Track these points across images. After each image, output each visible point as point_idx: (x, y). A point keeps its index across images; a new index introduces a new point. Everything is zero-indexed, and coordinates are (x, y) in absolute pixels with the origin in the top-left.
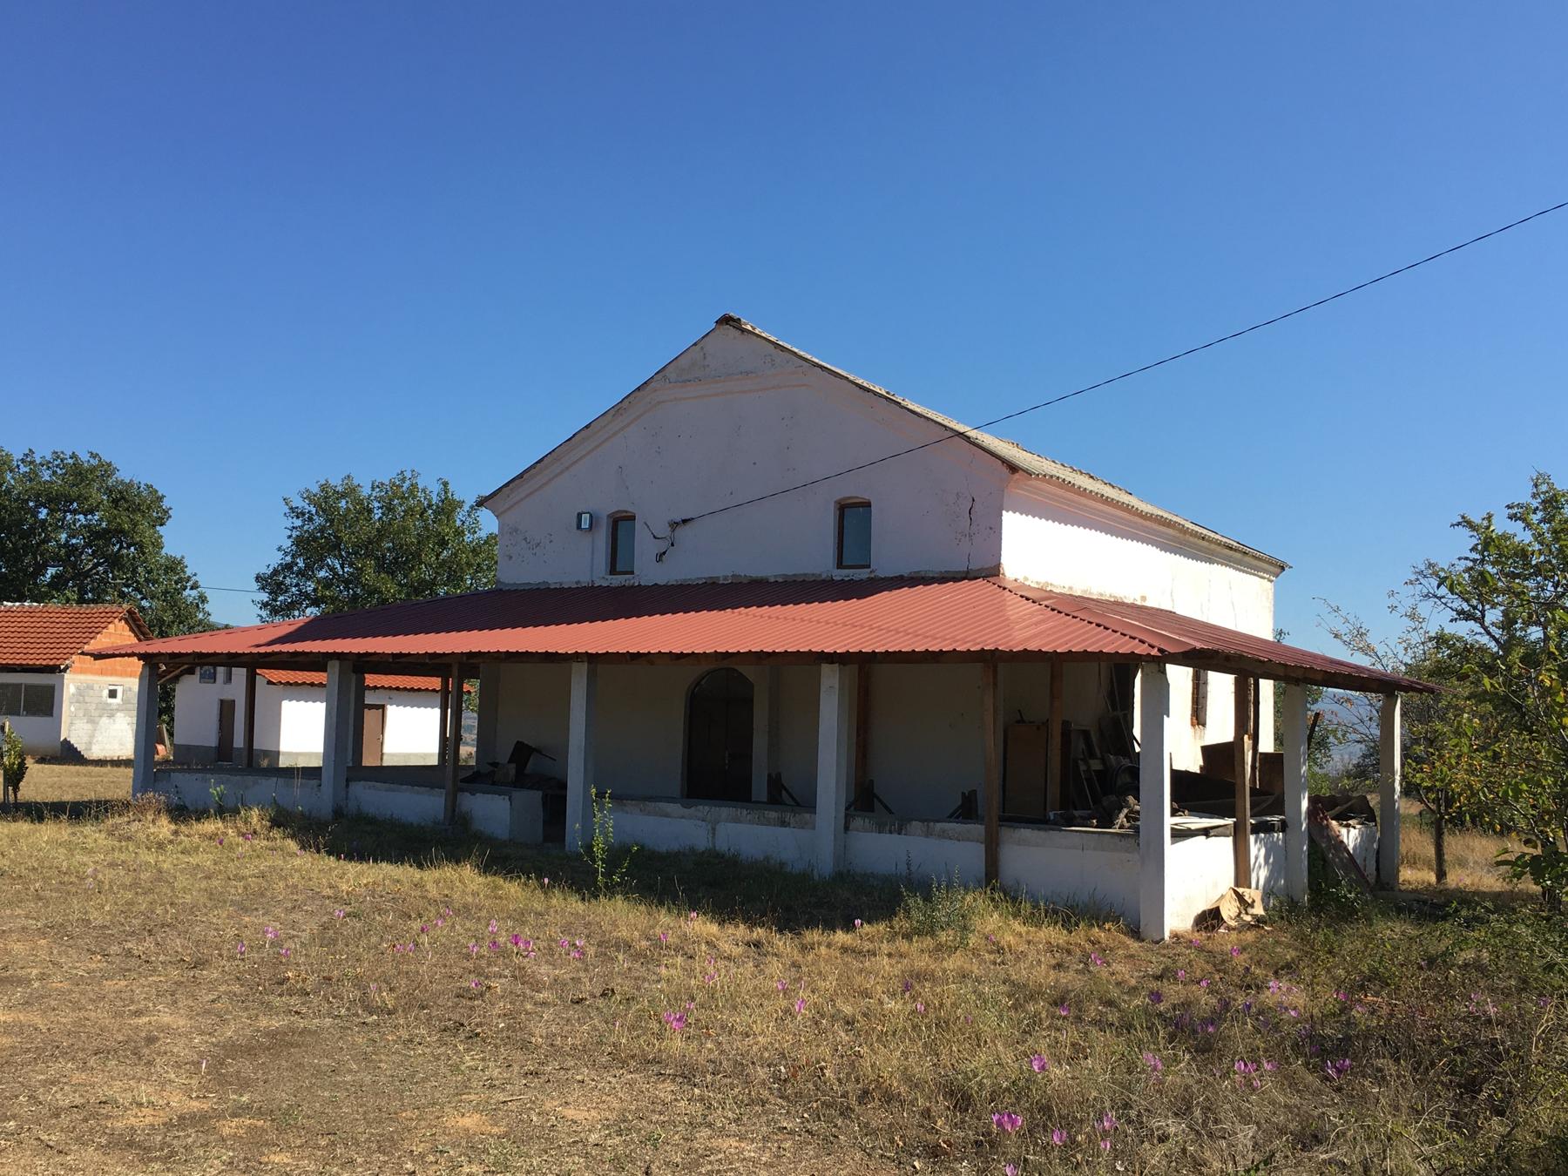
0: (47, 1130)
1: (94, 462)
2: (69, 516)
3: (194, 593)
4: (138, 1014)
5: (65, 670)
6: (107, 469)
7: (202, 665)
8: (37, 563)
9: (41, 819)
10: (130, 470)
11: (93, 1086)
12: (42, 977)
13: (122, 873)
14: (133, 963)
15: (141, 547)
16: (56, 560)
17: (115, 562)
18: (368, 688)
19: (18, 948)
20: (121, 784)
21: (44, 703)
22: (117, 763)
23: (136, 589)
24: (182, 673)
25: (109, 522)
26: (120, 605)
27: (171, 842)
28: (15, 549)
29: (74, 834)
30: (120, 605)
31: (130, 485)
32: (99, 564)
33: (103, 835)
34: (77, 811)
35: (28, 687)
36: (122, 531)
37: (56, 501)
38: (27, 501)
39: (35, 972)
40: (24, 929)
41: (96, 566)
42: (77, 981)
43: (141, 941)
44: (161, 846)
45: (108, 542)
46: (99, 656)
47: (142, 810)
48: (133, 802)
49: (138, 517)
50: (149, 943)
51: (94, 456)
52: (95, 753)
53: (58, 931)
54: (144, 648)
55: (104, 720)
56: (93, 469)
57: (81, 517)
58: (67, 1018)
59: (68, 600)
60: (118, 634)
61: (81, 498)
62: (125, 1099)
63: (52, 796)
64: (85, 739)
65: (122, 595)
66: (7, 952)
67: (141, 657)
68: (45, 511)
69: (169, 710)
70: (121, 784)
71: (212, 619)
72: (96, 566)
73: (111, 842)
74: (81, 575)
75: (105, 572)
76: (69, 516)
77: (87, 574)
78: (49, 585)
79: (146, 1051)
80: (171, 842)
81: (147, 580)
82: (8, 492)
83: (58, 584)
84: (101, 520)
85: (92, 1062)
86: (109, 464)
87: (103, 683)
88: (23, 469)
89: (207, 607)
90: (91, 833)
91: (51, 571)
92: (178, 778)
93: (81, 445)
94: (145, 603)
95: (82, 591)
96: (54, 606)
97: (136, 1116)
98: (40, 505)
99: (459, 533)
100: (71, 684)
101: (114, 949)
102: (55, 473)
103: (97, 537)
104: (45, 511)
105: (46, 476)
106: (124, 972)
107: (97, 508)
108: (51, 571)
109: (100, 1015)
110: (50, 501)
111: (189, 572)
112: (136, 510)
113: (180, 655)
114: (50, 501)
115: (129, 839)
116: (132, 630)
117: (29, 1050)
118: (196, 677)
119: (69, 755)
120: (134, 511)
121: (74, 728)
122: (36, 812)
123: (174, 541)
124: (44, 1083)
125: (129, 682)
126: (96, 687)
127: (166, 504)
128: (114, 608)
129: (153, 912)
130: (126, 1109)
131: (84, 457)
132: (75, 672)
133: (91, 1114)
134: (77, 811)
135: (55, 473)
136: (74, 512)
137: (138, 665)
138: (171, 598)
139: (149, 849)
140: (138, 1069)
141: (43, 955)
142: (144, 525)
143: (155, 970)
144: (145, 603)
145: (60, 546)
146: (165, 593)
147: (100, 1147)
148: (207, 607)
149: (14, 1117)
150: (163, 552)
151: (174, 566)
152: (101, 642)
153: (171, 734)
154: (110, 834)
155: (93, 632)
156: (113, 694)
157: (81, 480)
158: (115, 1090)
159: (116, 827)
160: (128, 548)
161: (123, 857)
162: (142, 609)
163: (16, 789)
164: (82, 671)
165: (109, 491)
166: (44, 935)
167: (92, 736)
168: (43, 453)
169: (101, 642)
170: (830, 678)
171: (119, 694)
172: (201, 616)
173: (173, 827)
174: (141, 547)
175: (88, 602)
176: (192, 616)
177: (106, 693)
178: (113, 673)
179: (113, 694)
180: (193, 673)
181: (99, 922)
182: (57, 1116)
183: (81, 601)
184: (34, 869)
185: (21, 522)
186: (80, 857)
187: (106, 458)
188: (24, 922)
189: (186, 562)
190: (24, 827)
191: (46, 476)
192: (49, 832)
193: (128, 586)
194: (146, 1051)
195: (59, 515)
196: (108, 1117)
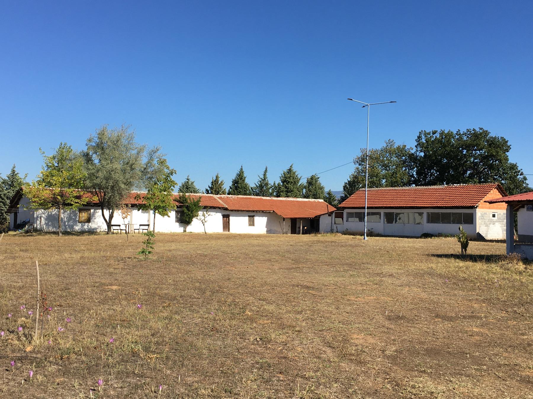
0: (498, 371)
1: (481, 131)
2: (474, 152)
3: (522, 177)
4: (523, 334)
5: (476, 208)
6: (486, 133)
7: (527, 205)
8: (464, 170)
9: (476, 261)
10: (494, 133)
11: (511, 358)
12: (486, 317)
13: (508, 282)
14: (517, 315)
15: (501, 161)
16: (470, 168)
17: (491, 167)
18: (113, 225)
19: (476, 306)
20: (502, 249)
21: (470, 219)
22: (497, 241)
23: (499, 177)
24: (520, 208)
25: (488, 153)
26: (494, 183)
27: (524, 272)
28: (456, 165)
29: (488, 267)
30: (494, 183)
31: (495, 138)
32: (486, 168)
33: (499, 268)
34: (489, 259)
35: (464, 214)
36: (493, 156)
37: (469, 147)
38: (459, 148)
39: (483, 315)
40: (477, 299)
41: (484, 169)
42: (499, 320)
43: (519, 308)
44: (520, 273)
45: (488, 160)
46: (491, 202)
47: (512, 259)
48: (508, 256)
49: (499, 149)
50: (522, 309)
51: (481, 129)
52: (488, 238)
53: (488, 301)
54: (507, 199)
55: (491, 225)
56: (481, 134)
57: (478, 152)
58: (497, 333)
59: (475, 182)
60: (494, 194)
61: (477, 145)
62: (524, 365)
63: (477, 253)
64: (485, 232)
65: (494, 179)
66: (472, 307)
67: (506, 202)
68: (465, 151)
69: (516, 221)
70: (502, 249)
71: (529, 186)
72: (484, 169)
73: (501, 271)
74: (479, 173)
75: (488, 171)
76: (474, 152)
77: (481, 172)
78: (468, 177)
79: (528, 349)
80: (524, 272)
81: (503, 173)
82: (453, 145)
83: (471, 176)
84: (485, 152)
85: (509, 349)
86: (487, 131)
87: (490, 212)
88: (457, 137)
89: (527, 182)
90: (494, 267)
91: (469, 172)
92: (524, 248)
93: (476, 126)
94: (503, 182)
95: (480, 179)
96: (471, 185)
97: (529, 372)
98: (463, 149)
99: (17, 180)
100: (479, 212)
101: (510, 310)
102: (468, 137)
103: (484, 158)
104: (465, 151)
105: (465, 138)
106: (515, 319)
107: (483, 148)
108: (469, 172)
109: (509, 333)
110: (466, 147)
111: (519, 169)
112: (499, 147)
113: (521, 201)
114: (466, 147)
115: (508, 269)
116: (499, 192)
117: (485, 342)
118: (525, 209)
119: (480, 238)
120: (497, 148)
121: (481, 228)
122: (474, 258)
123: (512, 157)
124: (494, 354)
125: (502, 211)
126: (488, 213)
127: (509, 144)
128: (492, 184)
129: (522, 297)
130: (525, 369)
131: (478, 130)
132: (480, 208)
133: (513, 370)
134: (489, 259)
135: (468, 137)
136: (476, 150)
137: (505, 205)
138: (513, 179)
139: (516, 274)
140: (527, 355)
141: (484, 309)
142: (501, 153)
143: (526, 319)
144: (503, 182)
145: (471, 163)
146: (510, 177)
147: (517, 381)
148: (527, 182)
149: (485, 365)
150: (509, 162)
151: (513, 167)
152: (489, 197)
153: (516, 231)
154: (501, 267)
155: (486, 193)
156: (494, 216)
157: (477, 138)
158: (519, 361)
159: (503, 265)
160: (496, 161)
161: (507, 276)
162: (502, 184)
163: (466, 250)
164: (482, 208)
165: (488, 141)
166: (484, 302)
167: (487, 231)
168: (463, 130)
169: (489, 197)
170: (12, 228)
171: (496, 216)
172: (525, 185)
173: (524, 266)
174: (500, 161)
175: (483, 182)
176: (522, 185)
177: (491, 216)
178: (493, 208)
179: (494, 216)
180: (524, 207)
181: (503, 299)
182: (500, 367)
183: (480, 182)
184: (476, 278)
185: (458, 155)
186: (491, 275)
187: (485, 129)
188: (476, 297)
189: (518, 165)
190: (470, 263)
191: (465, 138)
192: (479, 266)
193: (496, 176)
194: (528, 349)
195: (470, 152)
196: (518, 370)
